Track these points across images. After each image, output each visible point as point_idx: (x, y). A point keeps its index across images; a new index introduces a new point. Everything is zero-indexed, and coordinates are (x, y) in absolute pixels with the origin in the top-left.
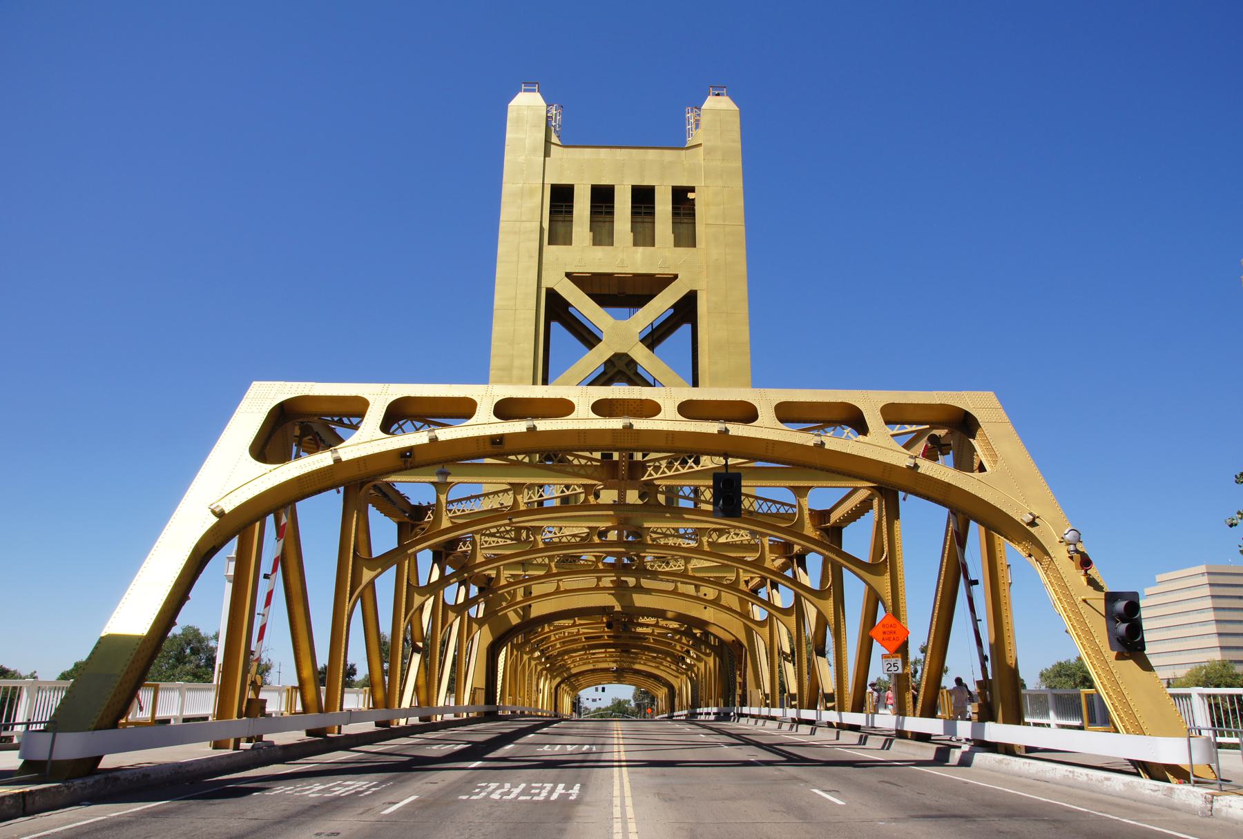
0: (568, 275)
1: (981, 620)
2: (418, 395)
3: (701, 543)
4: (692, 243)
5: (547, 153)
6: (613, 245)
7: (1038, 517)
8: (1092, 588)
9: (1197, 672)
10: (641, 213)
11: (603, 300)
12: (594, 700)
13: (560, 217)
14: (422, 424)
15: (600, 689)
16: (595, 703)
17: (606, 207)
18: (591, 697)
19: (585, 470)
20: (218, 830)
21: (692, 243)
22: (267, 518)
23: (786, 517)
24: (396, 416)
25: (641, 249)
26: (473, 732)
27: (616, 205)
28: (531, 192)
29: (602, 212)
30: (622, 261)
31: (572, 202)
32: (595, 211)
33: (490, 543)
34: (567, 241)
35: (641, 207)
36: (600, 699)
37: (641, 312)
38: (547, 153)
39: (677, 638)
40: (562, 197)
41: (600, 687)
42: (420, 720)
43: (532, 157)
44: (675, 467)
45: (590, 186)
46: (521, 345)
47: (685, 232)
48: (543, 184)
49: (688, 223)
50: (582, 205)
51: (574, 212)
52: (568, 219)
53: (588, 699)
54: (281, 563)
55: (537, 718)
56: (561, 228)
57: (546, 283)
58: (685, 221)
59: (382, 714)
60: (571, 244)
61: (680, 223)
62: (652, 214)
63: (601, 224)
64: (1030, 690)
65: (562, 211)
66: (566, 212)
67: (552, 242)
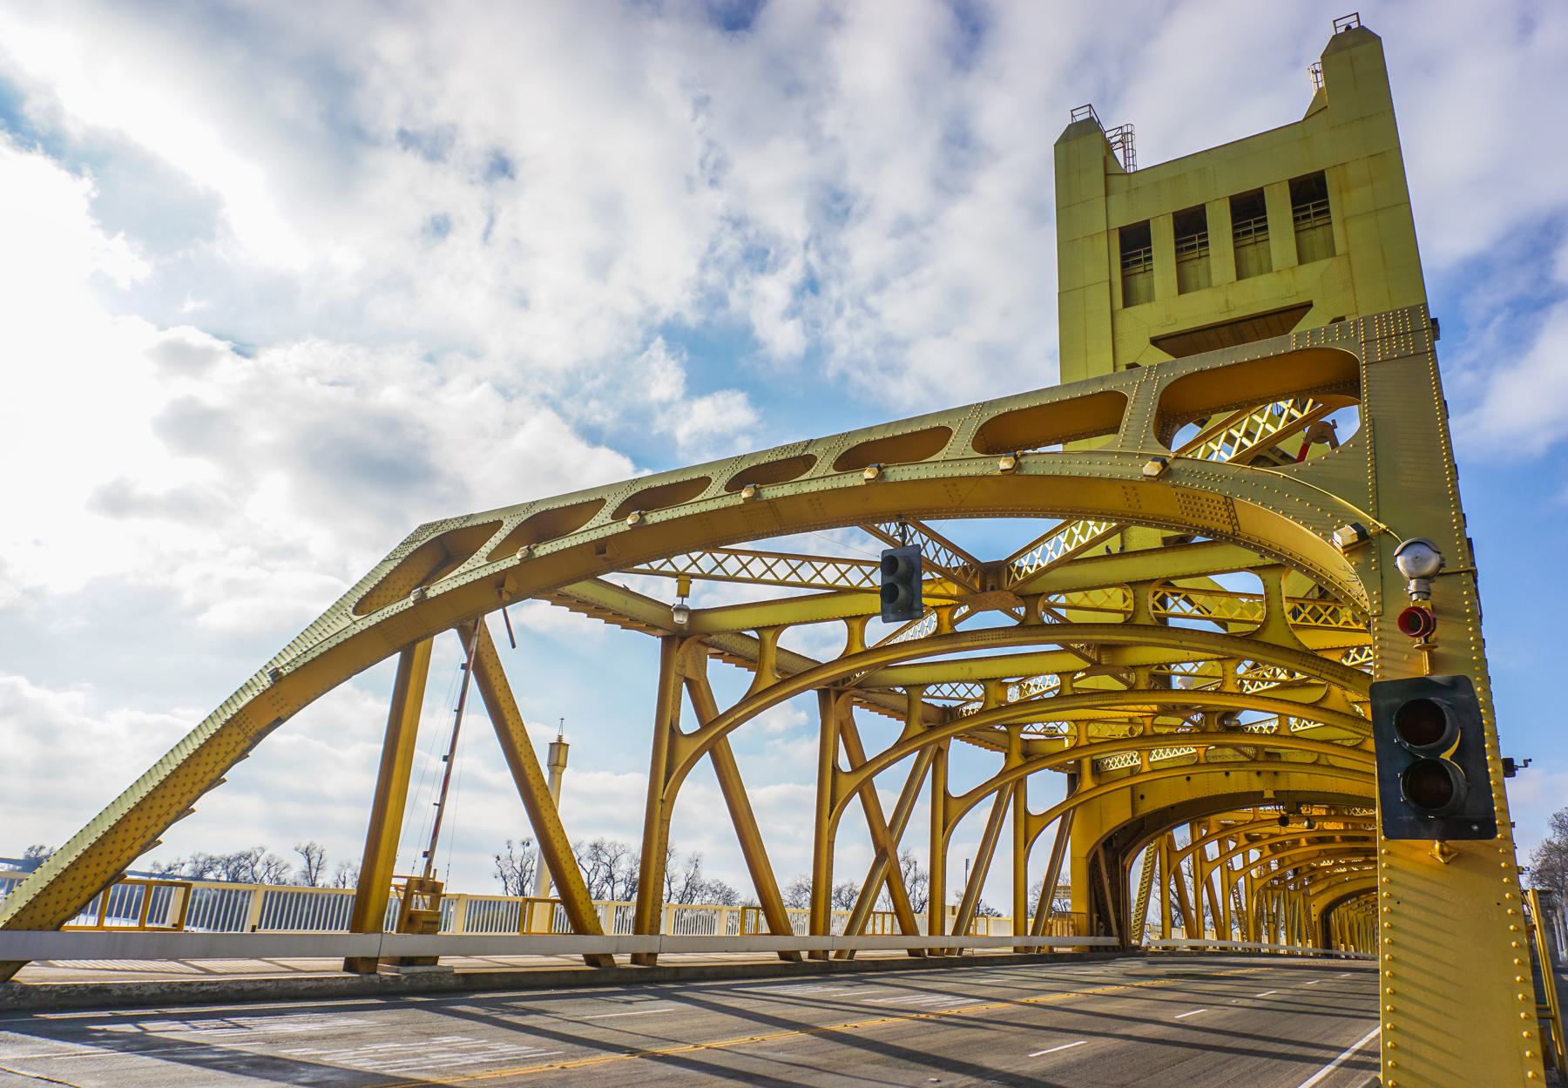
0: (1155, 342)
1: (435, 804)
8: (550, 603)
14: (850, 566)
19: (944, 588)
22: (435, 637)
29: (1310, 214)
39: (1333, 813)
45: (1287, 183)
52: (1148, 268)
56: (1140, 281)
58: (1318, 223)
63: (1196, 262)
64: (1504, 798)
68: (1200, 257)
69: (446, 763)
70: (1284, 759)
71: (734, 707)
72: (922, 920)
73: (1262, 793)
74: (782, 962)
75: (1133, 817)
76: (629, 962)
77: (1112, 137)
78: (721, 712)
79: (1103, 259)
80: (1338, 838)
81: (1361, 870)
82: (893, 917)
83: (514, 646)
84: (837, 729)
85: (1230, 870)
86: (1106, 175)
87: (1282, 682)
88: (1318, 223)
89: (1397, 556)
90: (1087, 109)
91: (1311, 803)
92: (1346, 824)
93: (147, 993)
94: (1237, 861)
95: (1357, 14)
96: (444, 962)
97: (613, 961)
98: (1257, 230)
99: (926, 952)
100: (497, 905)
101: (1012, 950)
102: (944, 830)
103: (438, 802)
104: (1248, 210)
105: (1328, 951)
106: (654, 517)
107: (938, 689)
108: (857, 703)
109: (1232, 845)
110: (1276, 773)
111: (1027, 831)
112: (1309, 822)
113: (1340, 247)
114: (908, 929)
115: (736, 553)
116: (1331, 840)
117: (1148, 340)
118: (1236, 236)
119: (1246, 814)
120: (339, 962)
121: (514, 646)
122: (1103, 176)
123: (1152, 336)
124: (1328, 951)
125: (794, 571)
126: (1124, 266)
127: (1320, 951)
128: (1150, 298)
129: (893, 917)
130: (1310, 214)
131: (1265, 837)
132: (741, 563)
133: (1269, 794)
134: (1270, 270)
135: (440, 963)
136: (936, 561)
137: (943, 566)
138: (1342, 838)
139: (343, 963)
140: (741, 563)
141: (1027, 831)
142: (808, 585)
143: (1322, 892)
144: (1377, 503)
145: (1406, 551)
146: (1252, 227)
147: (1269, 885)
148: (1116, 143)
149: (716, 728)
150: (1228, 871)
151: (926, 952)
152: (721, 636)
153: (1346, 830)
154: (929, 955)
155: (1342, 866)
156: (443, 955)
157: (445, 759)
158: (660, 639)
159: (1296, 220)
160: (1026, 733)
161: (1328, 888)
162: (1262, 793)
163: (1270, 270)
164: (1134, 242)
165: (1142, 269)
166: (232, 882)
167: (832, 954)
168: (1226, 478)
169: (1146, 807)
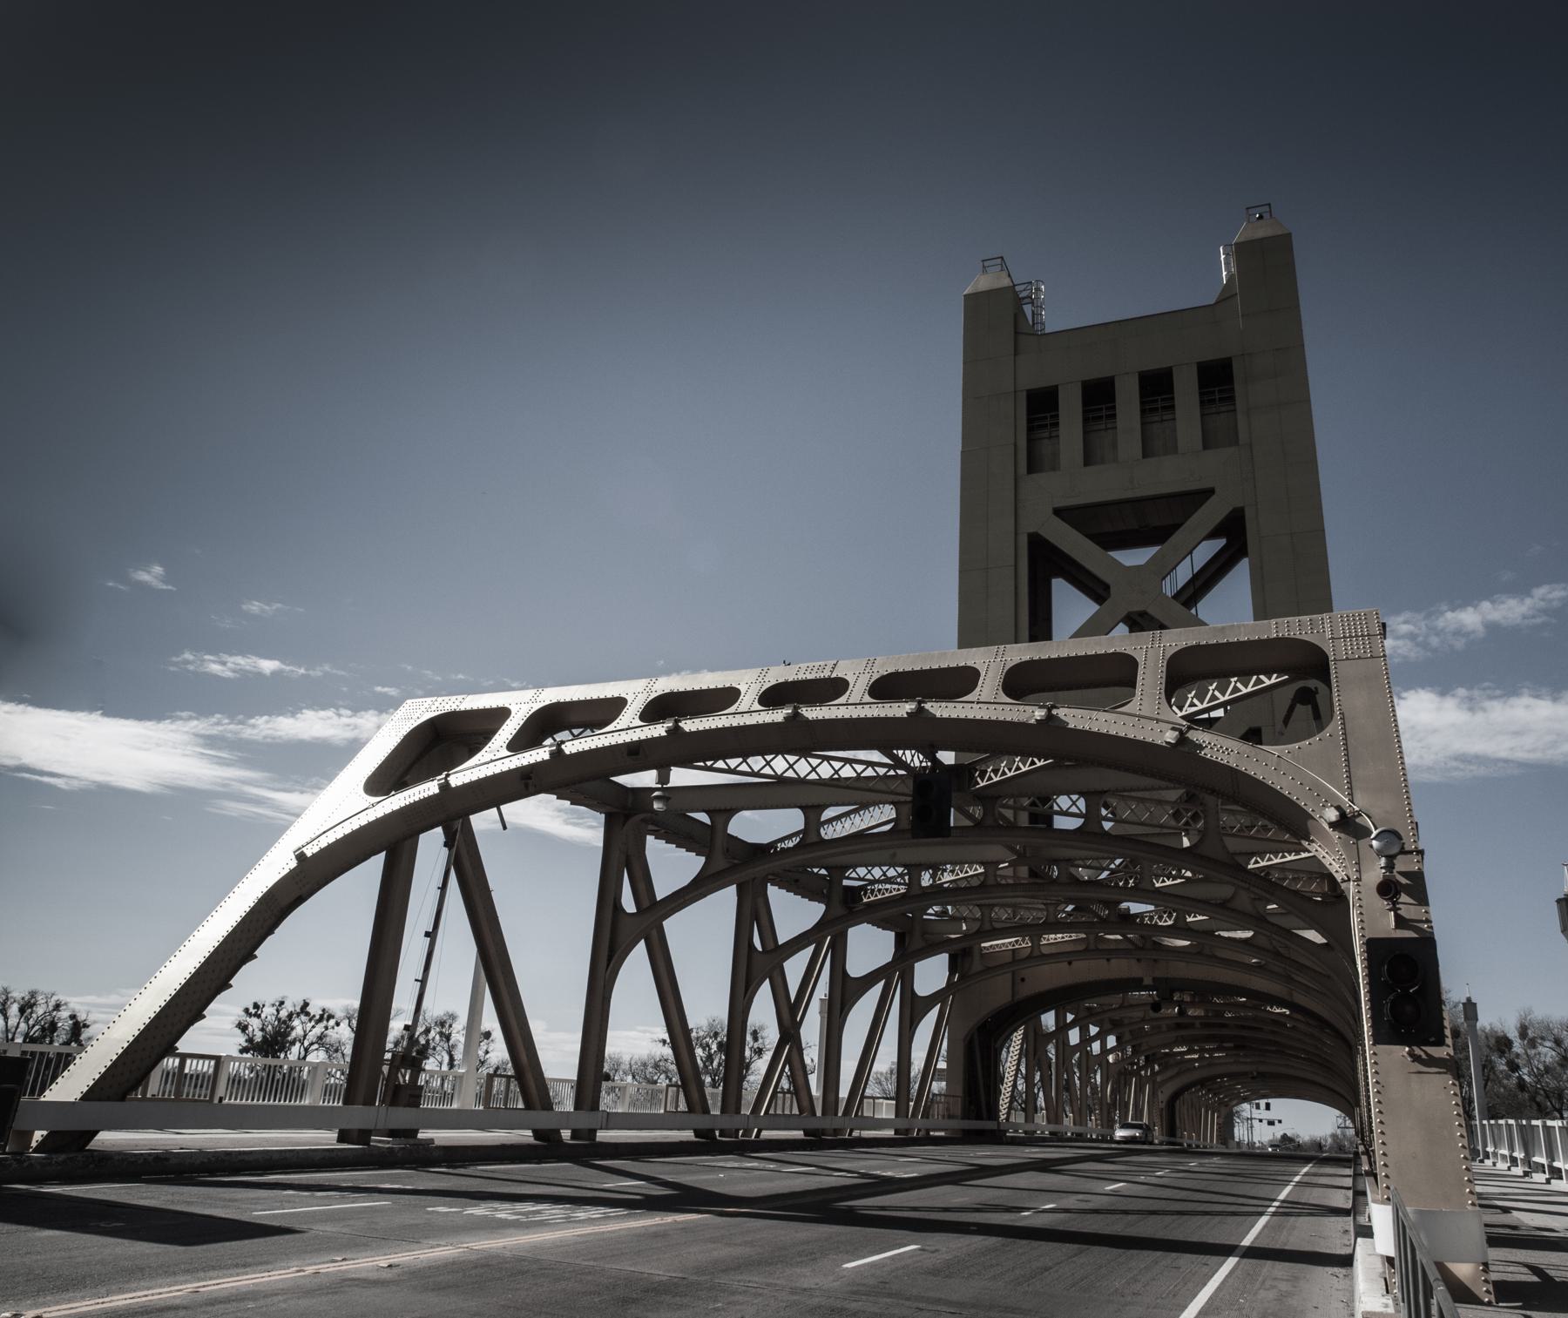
0: (1058, 512)
1: (416, 980)
3: (904, 880)
10: (1157, 409)
12: (1271, 1123)
15: (1263, 1105)
16: (1272, 1127)
17: (1107, 409)
20: (901, 1302)
24: (655, 710)
26: (1230, 1178)
29: (1215, 399)
33: (891, 892)
34: (1172, 448)
35: (1046, 418)
36: (1280, 1122)
41: (1263, 1102)
42: (805, 1135)
44: (1001, 771)
45: (1080, 384)
49: (1227, 411)
55: (1113, 1146)
57: (1029, 526)
58: (1223, 409)
59: (903, 1124)
66: (1163, 408)
68: (1107, 429)
69: (429, 939)
72: (714, 1095)
73: (1141, 980)
74: (697, 1139)
75: (1013, 1000)
76: (569, 1138)
77: (1021, 291)
79: (1011, 421)
80: (1198, 1025)
81: (1211, 1057)
82: (678, 1092)
84: (753, 913)
86: (1016, 333)
87: (1188, 879)
89: (1372, 839)
90: (999, 261)
91: (1181, 990)
92: (1206, 1011)
93: (198, 1162)
94: (1074, 1036)
95: (1269, 205)
96: (423, 1135)
97: (561, 1136)
98: (1164, 408)
99: (717, 1133)
101: (893, 1133)
102: (609, 960)
103: (420, 978)
104: (1156, 387)
105: (1172, 1139)
106: (689, 725)
109: (1070, 1017)
110: (1155, 961)
111: (914, 1009)
112: (1179, 1006)
113: (1243, 436)
114: (697, 1104)
116: (1190, 1026)
117: (1051, 511)
118: (1143, 412)
119: (1115, 1000)
120: (334, 1135)
122: (1013, 333)
123: (1056, 506)
124: (1172, 1139)
126: (1030, 429)
127: (1165, 1138)
128: (1055, 467)
129: (678, 1092)
130: (1215, 399)
131: (1126, 1021)
133: (1148, 981)
134: (1175, 450)
135: (420, 1136)
136: (904, 758)
137: (909, 762)
138: (1201, 1024)
139: (337, 1135)
141: (914, 1009)
142: (847, 761)
143: (1171, 1078)
144: (1350, 788)
145: (1379, 837)
146: (1159, 405)
147: (1123, 1070)
148: (1024, 298)
149: (655, 911)
150: (1063, 1044)
151: (717, 1133)
152: (786, 842)
153: (1206, 1016)
154: (720, 1136)
155: (1195, 1052)
156: (767, 1129)
157: (427, 934)
158: (603, 815)
159: (1202, 402)
160: (848, 878)
161: (1178, 1074)
162: (1141, 980)
163: (1175, 450)
164: (1042, 405)
166: (29, 1042)
167: (1069, 1134)
168: (1232, 751)
169: (1026, 991)
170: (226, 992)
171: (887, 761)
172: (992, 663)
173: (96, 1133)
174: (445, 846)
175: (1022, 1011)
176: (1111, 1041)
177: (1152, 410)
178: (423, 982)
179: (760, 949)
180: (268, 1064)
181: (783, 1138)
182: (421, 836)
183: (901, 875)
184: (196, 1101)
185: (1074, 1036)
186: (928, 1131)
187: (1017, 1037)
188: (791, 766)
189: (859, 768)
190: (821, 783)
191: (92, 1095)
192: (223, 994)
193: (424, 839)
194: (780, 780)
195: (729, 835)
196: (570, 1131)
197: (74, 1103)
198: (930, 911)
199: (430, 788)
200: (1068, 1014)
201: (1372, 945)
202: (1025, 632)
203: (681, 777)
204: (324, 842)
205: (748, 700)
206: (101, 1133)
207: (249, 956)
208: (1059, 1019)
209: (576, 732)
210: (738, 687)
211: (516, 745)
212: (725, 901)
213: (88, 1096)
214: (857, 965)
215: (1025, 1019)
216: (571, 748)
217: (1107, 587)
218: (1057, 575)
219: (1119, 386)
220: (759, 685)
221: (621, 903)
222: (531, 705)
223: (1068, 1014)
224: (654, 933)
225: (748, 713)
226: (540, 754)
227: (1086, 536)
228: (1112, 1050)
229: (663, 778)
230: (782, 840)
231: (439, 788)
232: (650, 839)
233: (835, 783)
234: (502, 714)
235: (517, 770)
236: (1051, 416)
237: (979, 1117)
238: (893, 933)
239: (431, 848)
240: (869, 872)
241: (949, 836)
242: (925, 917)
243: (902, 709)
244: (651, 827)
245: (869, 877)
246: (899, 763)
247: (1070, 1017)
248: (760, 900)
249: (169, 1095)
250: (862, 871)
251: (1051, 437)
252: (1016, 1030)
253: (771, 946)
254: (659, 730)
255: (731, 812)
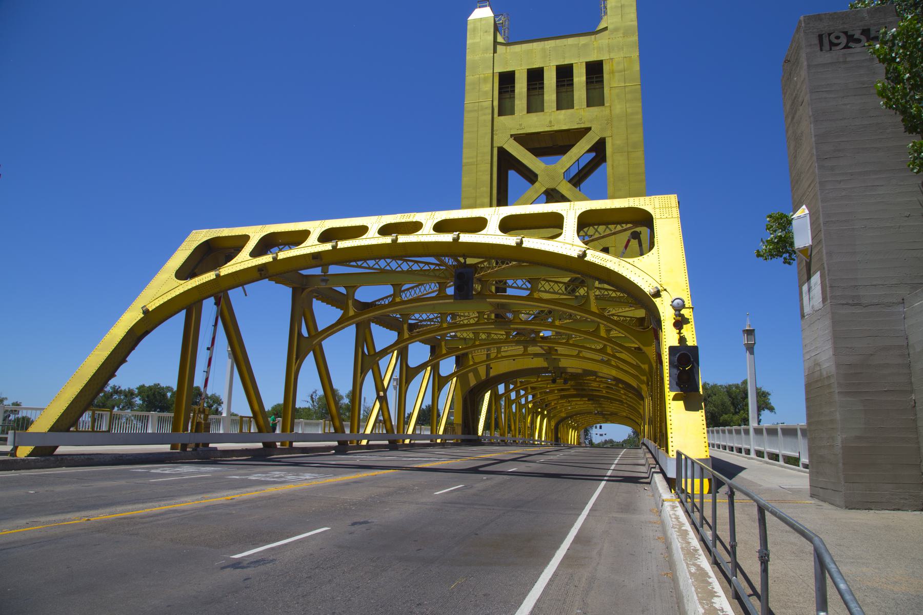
1: (204, 371)
2: (338, 226)
4: (601, 103)
5: (495, 51)
6: (543, 111)
7: (665, 290)
9: (768, 399)
11: (538, 152)
12: (601, 435)
13: (564, 89)
16: (601, 433)
18: (599, 433)
21: (601, 103)
23: (618, 300)
24: (325, 237)
25: (563, 112)
27: (545, 82)
28: (485, 80)
30: (551, 122)
31: (514, 84)
32: (589, 81)
35: (565, 81)
36: (605, 434)
37: (565, 158)
38: (495, 51)
40: (506, 80)
41: (598, 426)
43: (485, 55)
45: (555, 67)
46: (482, 189)
47: (595, 98)
48: (493, 73)
50: (521, 85)
51: (516, 91)
53: (597, 434)
54: (221, 318)
57: (497, 144)
58: (597, 87)
60: (543, 110)
61: (594, 89)
62: (602, 81)
65: (508, 91)
66: (539, 88)
67: (500, 114)
69: (209, 351)
70: (559, 352)
71: (333, 325)
78: (320, 329)
82: (330, 423)
83: (246, 295)
84: (363, 338)
85: (520, 403)
88: (597, 87)
94: (523, 401)
96: (211, 445)
98: (568, 85)
100: (100, 416)
103: (206, 370)
105: (557, 443)
107: (428, 317)
108: (315, 297)
111: (439, 382)
115: (406, 261)
120: (169, 446)
121: (246, 295)
125: (388, 265)
132: (390, 266)
140: (390, 266)
142: (417, 262)
150: (508, 398)
151: (349, 442)
152: (381, 301)
157: (208, 349)
158: (291, 289)
165: (508, 96)
169: (493, 373)
170: (114, 378)
171: (437, 262)
172: (495, 215)
173: (57, 447)
174: (215, 304)
175: (490, 383)
176: (530, 398)
177: (534, 89)
178: (208, 372)
179: (367, 354)
180: (137, 414)
181: (324, 446)
182: (204, 301)
183: (436, 318)
184: (98, 432)
185: (513, 395)
186: (291, 443)
187: (487, 396)
188: (388, 265)
189: (422, 265)
190: (402, 272)
191: (55, 428)
192: (112, 379)
193: (205, 302)
194: (382, 271)
195: (355, 299)
196: (170, 445)
197: (45, 433)
198: (449, 335)
199: (210, 276)
200: (511, 385)
201: (671, 349)
202: (495, 201)
203: (334, 269)
204: (157, 303)
205: (428, 227)
206: (59, 447)
207: (124, 361)
208: (506, 387)
209: (281, 247)
210: (310, 230)
211: (255, 254)
212: (350, 331)
213: (52, 429)
214: (413, 362)
215: (492, 387)
216: (282, 255)
217: (536, 176)
218: (511, 169)
219: (576, 71)
220: (377, 224)
221: (301, 332)
222: (260, 233)
223: (511, 385)
224: (317, 348)
225: (372, 238)
226: (267, 259)
227: (527, 149)
228: (530, 402)
229: (325, 271)
230: (382, 299)
231: (216, 276)
232: (314, 300)
233: (410, 272)
234: (246, 238)
235: (255, 266)
236: (511, 87)
237: (469, 434)
238: (429, 346)
239: (209, 308)
240: (428, 317)
241: (472, 299)
242: (447, 338)
243: (447, 238)
244: (315, 294)
245: (421, 318)
246: (443, 263)
247: (512, 387)
248: (367, 331)
249: (88, 429)
250: (417, 316)
251: (510, 98)
252: (487, 392)
253: (372, 353)
254: (328, 246)
255: (355, 288)
